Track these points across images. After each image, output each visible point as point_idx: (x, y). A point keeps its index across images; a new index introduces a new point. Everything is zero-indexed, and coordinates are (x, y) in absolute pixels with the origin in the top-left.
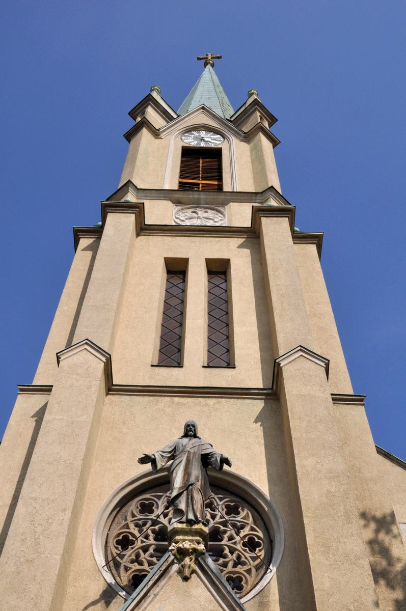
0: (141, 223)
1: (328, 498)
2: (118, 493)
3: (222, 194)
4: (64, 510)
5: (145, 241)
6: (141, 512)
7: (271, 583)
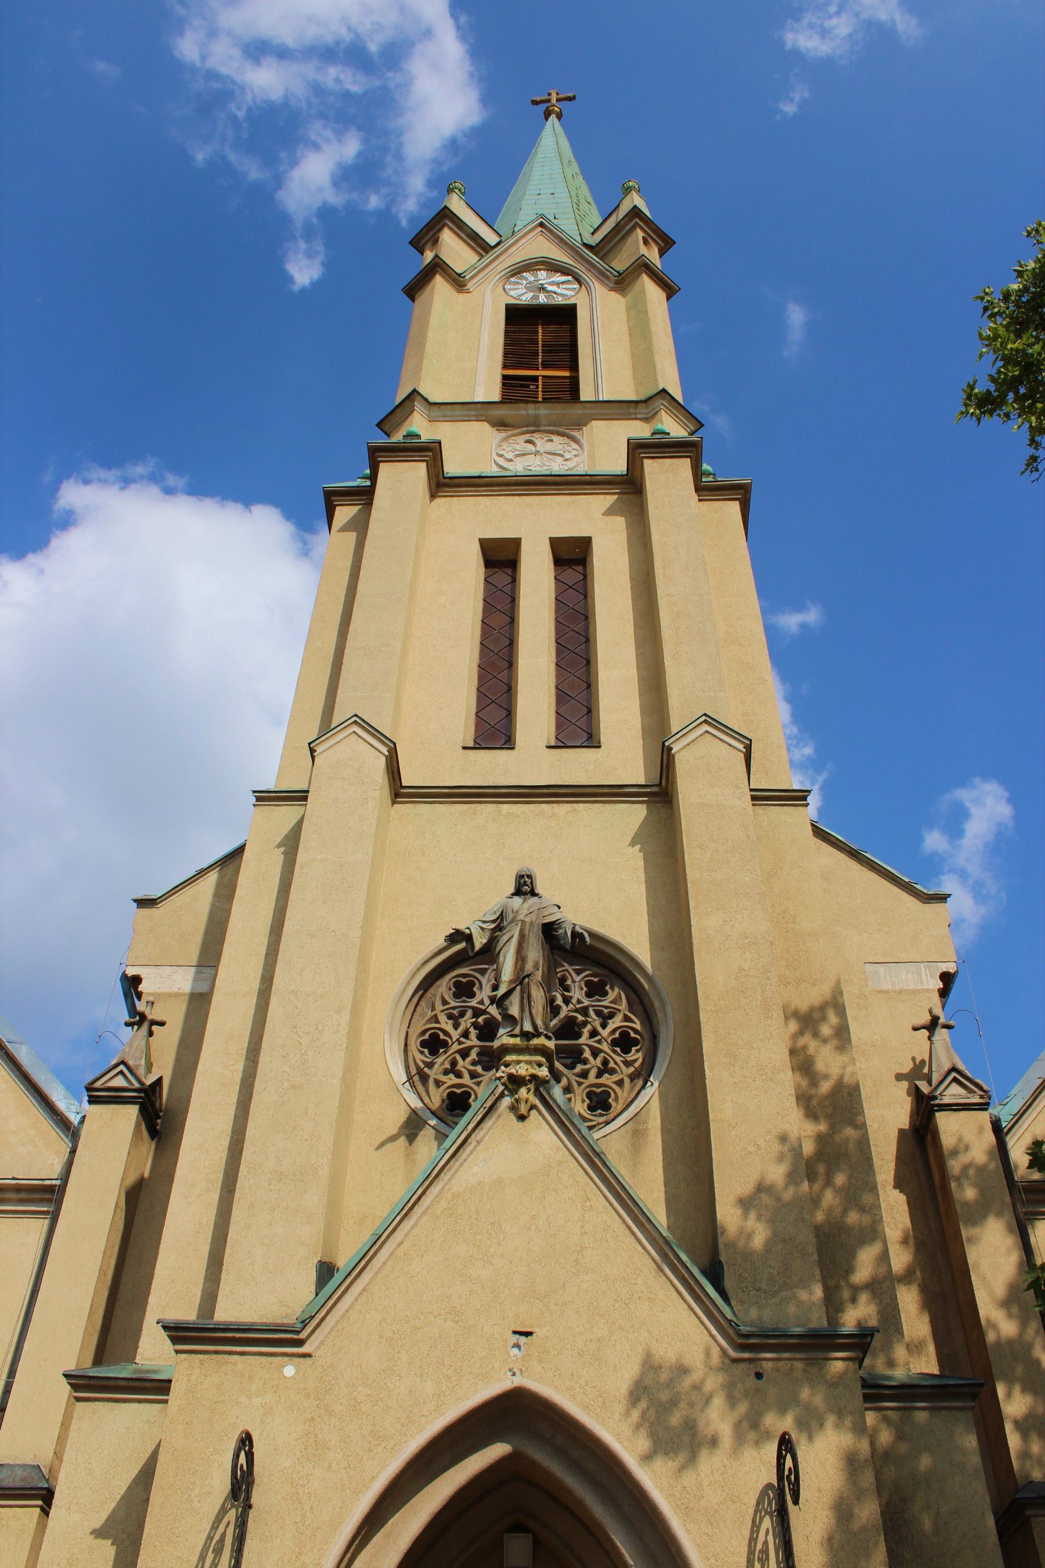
0: (437, 476)
1: (739, 979)
2: (418, 970)
3: (577, 405)
4: (339, 1011)
5: (447, 505)
6: (456, 996)
7: (650, 1102)
